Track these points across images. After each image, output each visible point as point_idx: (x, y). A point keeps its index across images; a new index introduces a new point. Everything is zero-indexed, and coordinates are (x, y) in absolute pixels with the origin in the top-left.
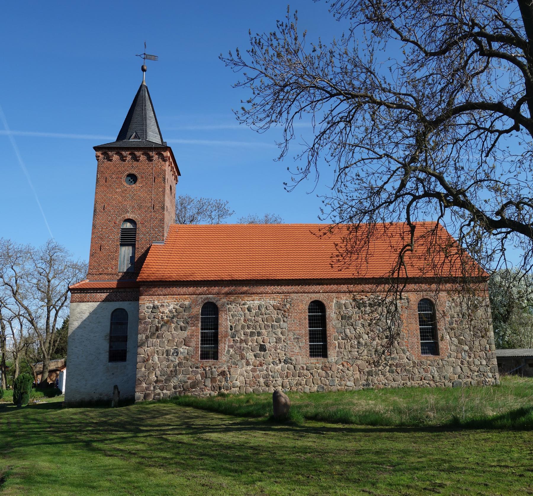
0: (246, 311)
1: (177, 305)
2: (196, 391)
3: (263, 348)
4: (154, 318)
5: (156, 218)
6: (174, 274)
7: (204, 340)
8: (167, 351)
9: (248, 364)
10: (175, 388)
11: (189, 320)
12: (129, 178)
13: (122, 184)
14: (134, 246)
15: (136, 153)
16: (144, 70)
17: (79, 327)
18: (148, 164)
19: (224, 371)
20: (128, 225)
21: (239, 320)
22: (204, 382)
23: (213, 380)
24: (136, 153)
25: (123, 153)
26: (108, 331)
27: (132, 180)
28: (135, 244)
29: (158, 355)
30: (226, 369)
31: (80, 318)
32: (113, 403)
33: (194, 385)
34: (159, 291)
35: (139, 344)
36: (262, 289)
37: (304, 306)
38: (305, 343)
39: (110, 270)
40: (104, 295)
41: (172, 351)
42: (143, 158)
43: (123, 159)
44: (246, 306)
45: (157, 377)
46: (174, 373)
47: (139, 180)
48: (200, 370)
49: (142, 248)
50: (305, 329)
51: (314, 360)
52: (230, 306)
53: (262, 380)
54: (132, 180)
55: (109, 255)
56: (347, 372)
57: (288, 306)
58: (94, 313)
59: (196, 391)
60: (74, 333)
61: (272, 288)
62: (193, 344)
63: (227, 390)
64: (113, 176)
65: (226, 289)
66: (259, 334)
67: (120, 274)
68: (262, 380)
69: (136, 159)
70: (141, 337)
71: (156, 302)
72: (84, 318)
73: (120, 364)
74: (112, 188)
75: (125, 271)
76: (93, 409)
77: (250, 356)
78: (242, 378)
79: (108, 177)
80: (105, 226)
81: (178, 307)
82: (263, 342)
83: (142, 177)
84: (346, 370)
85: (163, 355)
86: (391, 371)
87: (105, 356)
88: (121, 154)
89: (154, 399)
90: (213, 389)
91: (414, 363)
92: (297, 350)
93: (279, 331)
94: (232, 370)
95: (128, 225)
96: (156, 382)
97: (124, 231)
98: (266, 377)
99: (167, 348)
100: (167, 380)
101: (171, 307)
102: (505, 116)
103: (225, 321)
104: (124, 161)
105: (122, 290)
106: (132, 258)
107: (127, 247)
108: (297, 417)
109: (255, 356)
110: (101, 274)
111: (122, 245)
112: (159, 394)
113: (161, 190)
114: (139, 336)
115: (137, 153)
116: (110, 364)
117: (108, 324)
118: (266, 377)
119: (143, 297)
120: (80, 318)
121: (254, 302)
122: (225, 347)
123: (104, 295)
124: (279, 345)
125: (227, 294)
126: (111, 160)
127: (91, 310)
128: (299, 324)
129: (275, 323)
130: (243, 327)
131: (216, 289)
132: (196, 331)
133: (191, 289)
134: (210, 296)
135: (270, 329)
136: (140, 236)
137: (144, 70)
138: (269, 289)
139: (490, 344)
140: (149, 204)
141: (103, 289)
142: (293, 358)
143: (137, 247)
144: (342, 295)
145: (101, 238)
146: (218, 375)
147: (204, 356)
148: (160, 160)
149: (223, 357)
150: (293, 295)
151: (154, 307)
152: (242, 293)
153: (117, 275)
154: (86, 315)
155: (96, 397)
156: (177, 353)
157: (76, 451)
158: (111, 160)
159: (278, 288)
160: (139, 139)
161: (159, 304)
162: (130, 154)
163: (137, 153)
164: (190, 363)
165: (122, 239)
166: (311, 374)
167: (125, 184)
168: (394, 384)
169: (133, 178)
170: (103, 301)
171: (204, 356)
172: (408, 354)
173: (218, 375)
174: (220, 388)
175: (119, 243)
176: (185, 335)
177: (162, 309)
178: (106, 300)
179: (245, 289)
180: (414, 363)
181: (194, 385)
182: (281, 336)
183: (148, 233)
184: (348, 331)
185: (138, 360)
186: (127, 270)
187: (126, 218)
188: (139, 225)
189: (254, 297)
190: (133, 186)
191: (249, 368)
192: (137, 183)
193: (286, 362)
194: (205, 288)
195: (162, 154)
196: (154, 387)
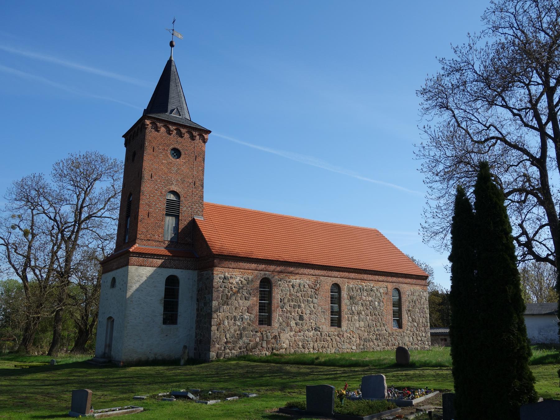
0: (291, 288)
1: (242, 277)
2: (257, 352)
3: (301, 318)
4: (225, 287)
5: (197, 194)
6: (241, 251)
7: (261, 310)
8: (235, 317)
9: (291, 331)
10: (240, 348)
11: (251, 291)
12: (173, 152)
14: (177, 217)
15: (182, 129)
16: (172, 45)
17: (137, 290)
19: (276, 336)
20: (172, 197)
21: (286, 294)
22: (262, 344)
23: (268, 343)
24: (182, 129)
26: (163, 294)
27: (175, 154)
28: (179, 216)
29: (228, 320)
30: (277, 334)
31: (138, 281)
32: (182, 362)
33: (255, 347)
34: (233, 265)
35: (213, 310)
36: (302, 270)
37: (328, 287)
38: (328, 316)
39: (157, 237)
40: (160, 262)
41: (239, 317)
42: (187, 136)
43: (169, 132)
44: (291, 283)
45: (227, 339)
46: (241, 336)
47: (183, 156)
48: (259, 334)
49: (185, 220)
50: (327, 306)
51: (333, 329)
52: (280, 282)
53: (300, 344)
54: (175, 154)
55: (156, 223)
56: (353, 339)
57: (318, 285)
58: (151, 277)
59: (257, 352)
60: (132, 295)
61: (309, 270)
62: (254, 312)
63: (277, 351)
64: (160, 147)
65: (278, 269)
66: (299, 307)
67: (167, 242)
68: (300, 344)
70: (215, 303)
71: (227, 274)
72: (142, 282)
73: (172, 327)
74: (159, 159)
75: (169, 240)
76: (173, 367)
77: (293, 323)
78: (287, 342)
79: (156, 148)
80: (152, 194)
81: (243, 280)
82: (302, 313)
84: (351, 337)
85: (231, 320)
86: (376, 339)
87: (160, 319)
89: (224, 357)
90: (268, 349)
91: (389, 333)
92: (323, 320)
93: (312, 305)
94: (281, 335)
95: (172, 197)
96: (226, 343)
97: (169, 202)
98: (303, 341)
99: (235, 314)
100: (235, 343)
101: (237, 280)
103: (277, 295)
104: (170, 134)
105: (176, 258)
106: (176, 228)
107: (171, 218)
108: (417, 365)
109: (296, 324)
110: (149, 240)
111: (167, 215)
112: (228, 354)
113: (200, 168)
114: (214, 302)
115: (183, 131)
116: (164, 326)
117: (163, 289)
118: (303, 341)
119: (216, 268)
120: (138, 281)
121: (296, 280)
122: (277, 316)
123: (160, 262)
124: (313, 316)
125: (281, 272)
126: (158, 131)
127: (149, 274)
128: (323, 301)
129: (309, 299)
130: (289, 301)
131: (272, 268)
132: (255, 300)
133: (253, 266)
134: (267, 272)
135: (306, 303)
136: (183, 209)
137: (172, 45)
138: (306, 271)
139: (427, 322)
140: (191, 181)
141: (158, 255)
142: (320, 327)
143: (180, 218)
144: (350, 281)
145: (149, 206)
146: (272, 339)
147: (261, 322)
149: (275, 324)
150: (322, 278)
151: (225, 278)
152: (288, 273)
153: (164, 243)
154: (144, 278)
155: (151, 357)
156: (242, 319)
157: (326, 383)
158: (158, 131)
159: (312, 271)
161: (229, 276)
162: (175, 129)
164: (251, 328)
165: (167, 209)
166: (331, 339)
168: (378, 348)
169: (177, 153)
170: (159, 267)
171: (261, 322)
172: (386, 327)
173: (272, 339)
174: (273, 349)
175: (165, 213)
176: (248, 304)
177: (231, 281)
178: (162, 266)
179: (292, 269)
180: (389, 333)
181: (255, 347)
182: (313, 309)
183: (190, 207)
184: (353, 308)
185: (212, 323)
186: (171, 239)
187: (171, 190)
188: (182, 199)
189: (297, 277)
190: (178, 160)
191: (292, 333)
193: (316, 330)
194: (264, 266)
196: (224, 348)
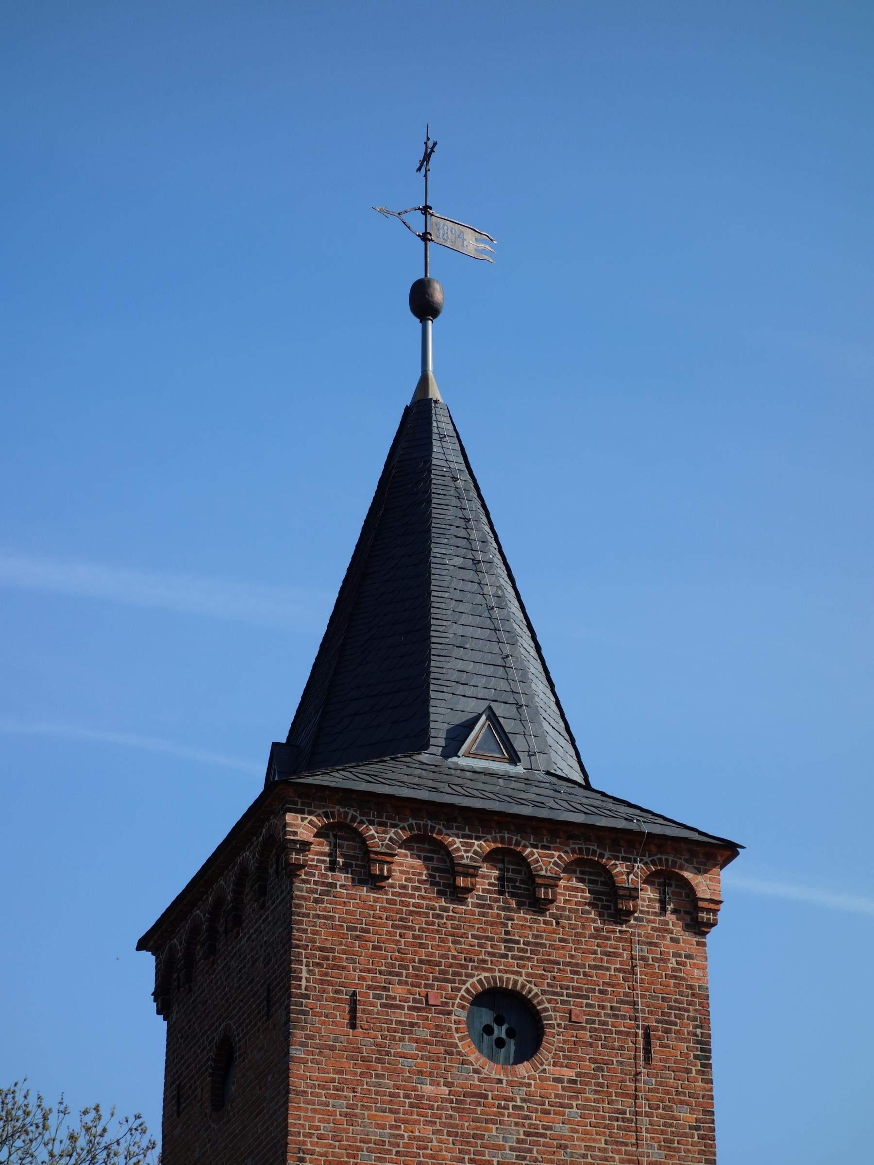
12: (486, 1016)
13: (450, 1050)
15: (533, 853)
16: (423, 304)
18: (597, 934)
25: (456, 843)
27: (500, 1032)
43: (449, 881)
47: (555, 1039)
54: (500, 1032)
64: (398, 991)
69: (527, 891)
74: (395, 1072)
83: (572, 1023)
88: (443, 850)
102: (700, 895)
104: (458, 895)
148: (670, 917)
158: (375, 882)
160: (514, 759)
162: (491, 858)
163: (545, 860)
167: (474, 1056)
169: (513, 1021)
192: (545, 1054)
195: (686, 884)
